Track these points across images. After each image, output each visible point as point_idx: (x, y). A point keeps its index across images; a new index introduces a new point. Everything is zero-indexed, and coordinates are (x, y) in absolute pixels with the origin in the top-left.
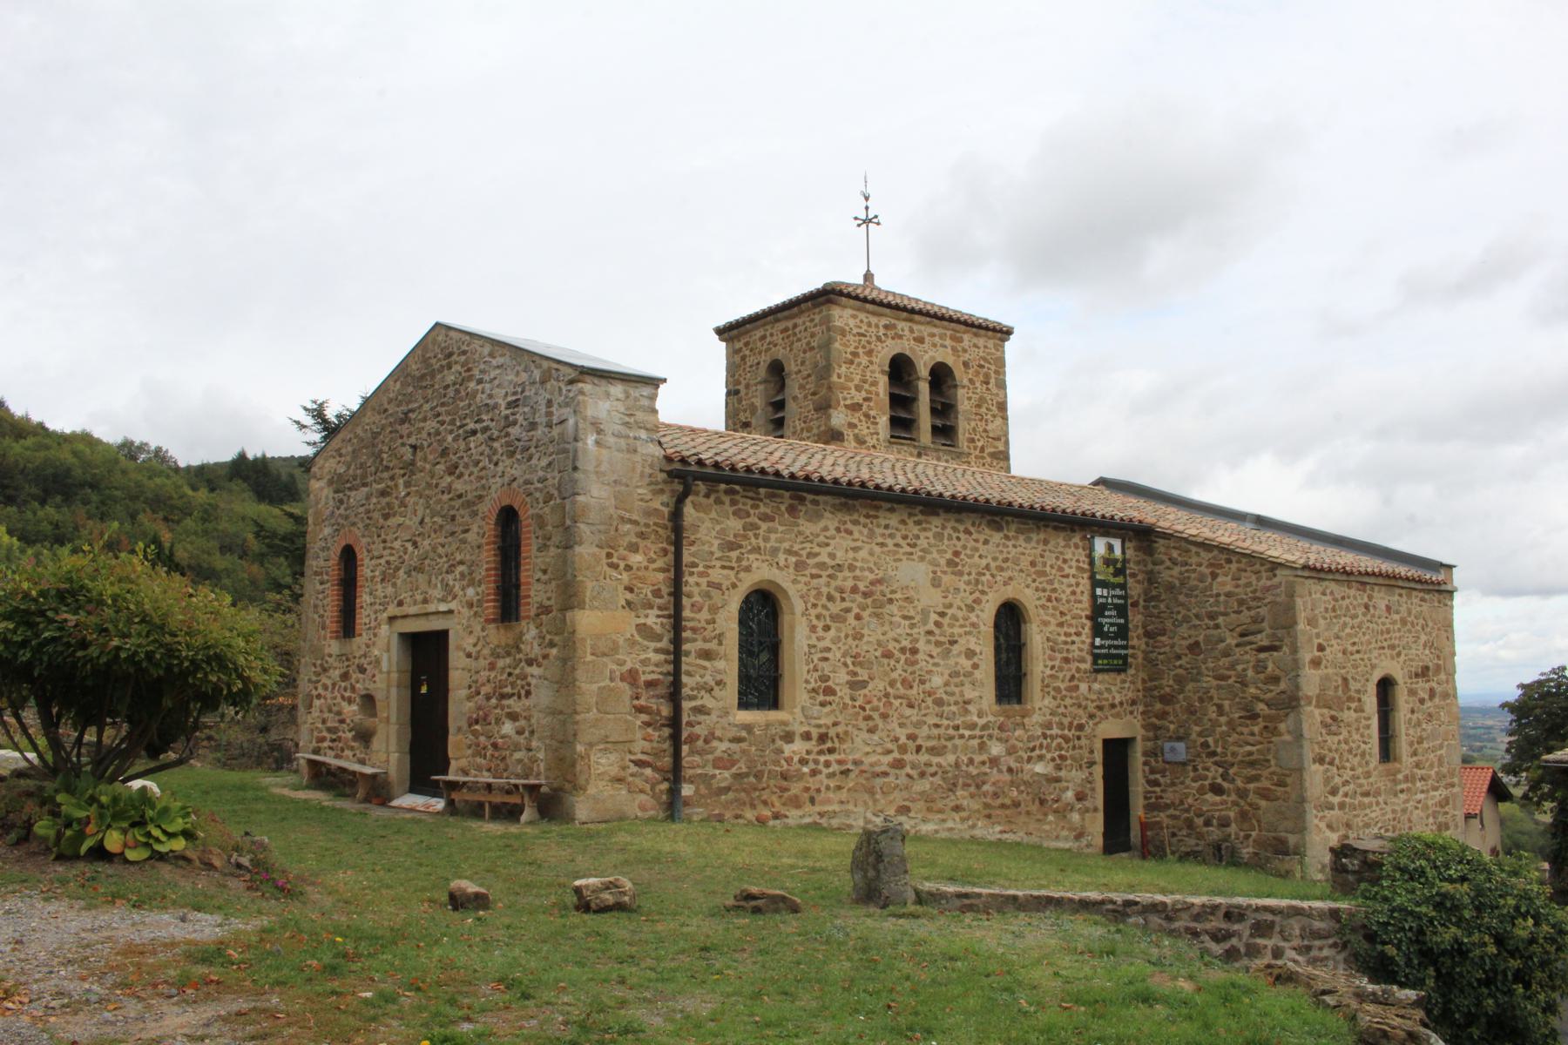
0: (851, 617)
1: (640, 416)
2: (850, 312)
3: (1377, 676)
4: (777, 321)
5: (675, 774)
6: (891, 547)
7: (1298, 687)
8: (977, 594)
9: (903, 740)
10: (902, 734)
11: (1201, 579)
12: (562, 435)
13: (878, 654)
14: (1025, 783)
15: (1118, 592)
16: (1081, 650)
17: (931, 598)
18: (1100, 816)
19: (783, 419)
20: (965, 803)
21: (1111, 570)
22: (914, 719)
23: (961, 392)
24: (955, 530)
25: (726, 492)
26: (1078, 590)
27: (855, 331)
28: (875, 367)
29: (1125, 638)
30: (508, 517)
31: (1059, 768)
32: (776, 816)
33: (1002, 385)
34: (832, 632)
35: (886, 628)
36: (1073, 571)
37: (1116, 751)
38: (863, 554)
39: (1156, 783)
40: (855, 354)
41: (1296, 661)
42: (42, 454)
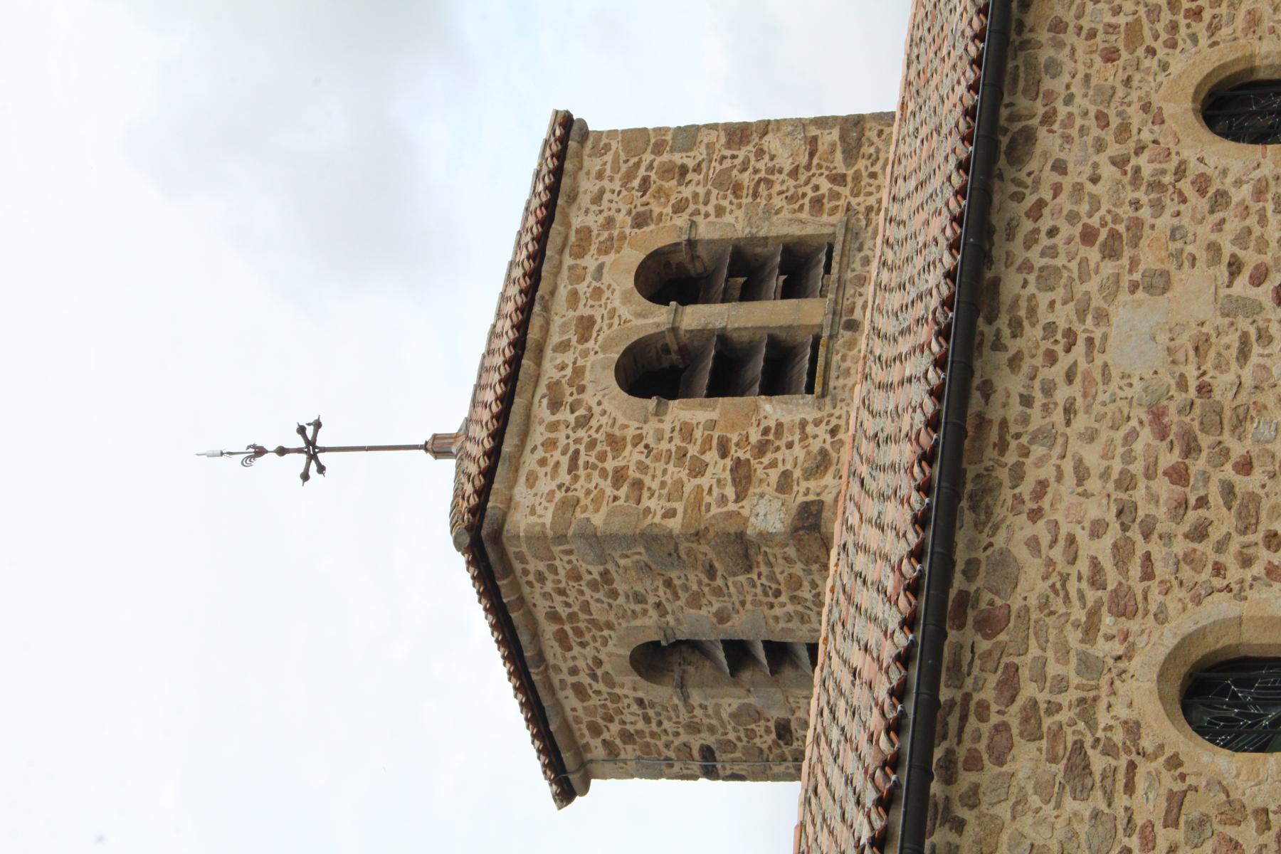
0: (1243, 484)
2: (520, 490)
4: (541, 657)
6: (1076, 390)
17: (1196, 296)
19: (768, 645)
23: (705, 231)
24: (1030, 241)
25: (949, 780)
27: (565, 478)
28: (649, 430)
33: (688, 136)
38: (1092, 456)
40: (619, 477)
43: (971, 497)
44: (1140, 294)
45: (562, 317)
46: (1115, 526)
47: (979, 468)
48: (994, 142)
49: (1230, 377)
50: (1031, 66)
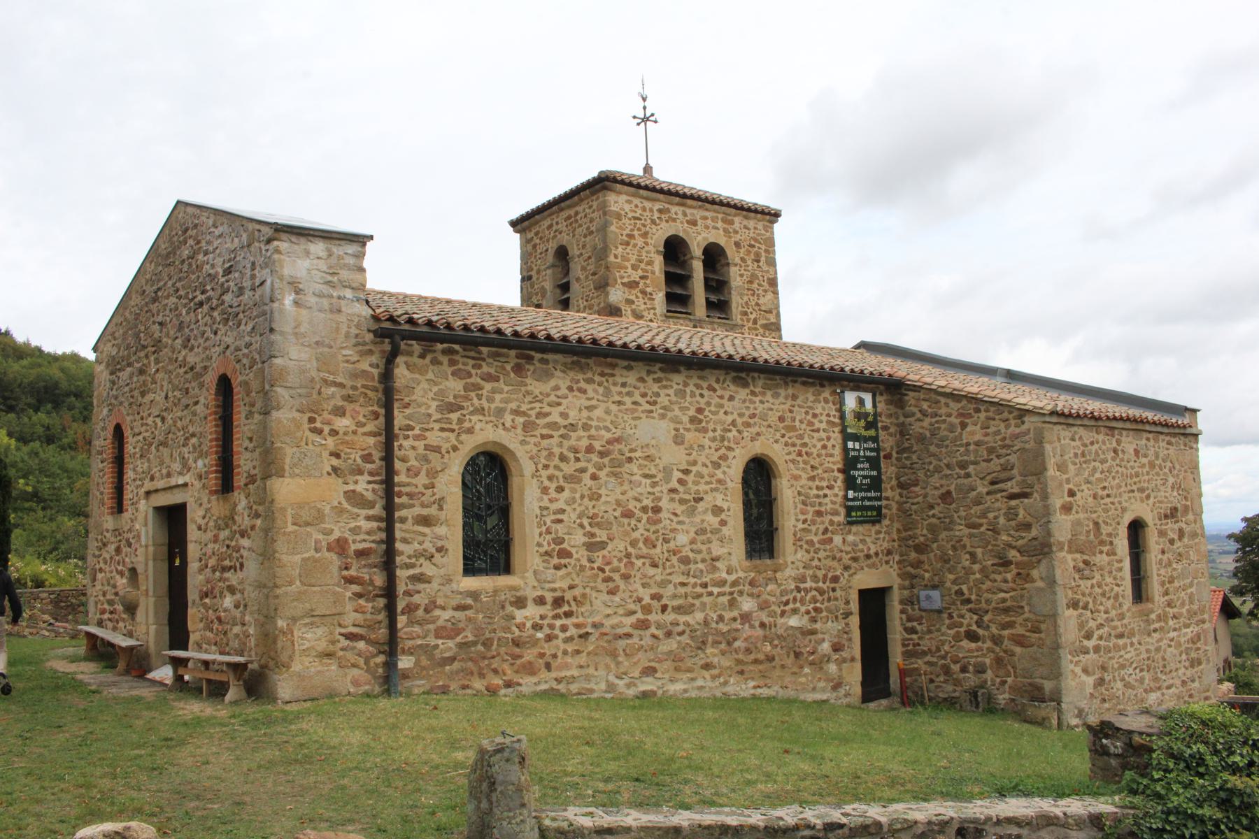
0: (586, 478)
1: (345, 274)
2: (624, 197)
3: (1127, 519)
4: (562, 210)
5: (391, 647)
6: (629, 405)
7: (1049, 534)
8: (723, 451)
9: (647, 600)
10: (646, 595)
11: (951, 428)
12: (262, 296)
13: (617, 514)
14: (779, 637)
15: (870, 445)
16: (833, 503)
17: (673, 456)
18: (858, 666)
19: (568, 299)
20: (716, 660)
21: (862, 423)
22: (658, 578)
23: (733, 271)
24: (698, 386)
25: (444, 352)
26: (829, 444)
27: (630, 215)
28: (651, 248)
29: (878, 489)
30: (225, 386)
31: (814, 620)
32: (508, 685)
33: (772, 263)
34: (566, 494)
35: (626, 487)
36: (823, 426)
37: (873, 601)
38: (598, 413)
39: (913, 631)
40: (631, 236)
41: (1046, 507)
42: (34, 372)
43: (579, 362)
44: (673, 432)
45: (698, 214)
46: (566, 423)
47: (592, 364)
48: (742, 371)
49: (635, 470)
50: (777, 386)
